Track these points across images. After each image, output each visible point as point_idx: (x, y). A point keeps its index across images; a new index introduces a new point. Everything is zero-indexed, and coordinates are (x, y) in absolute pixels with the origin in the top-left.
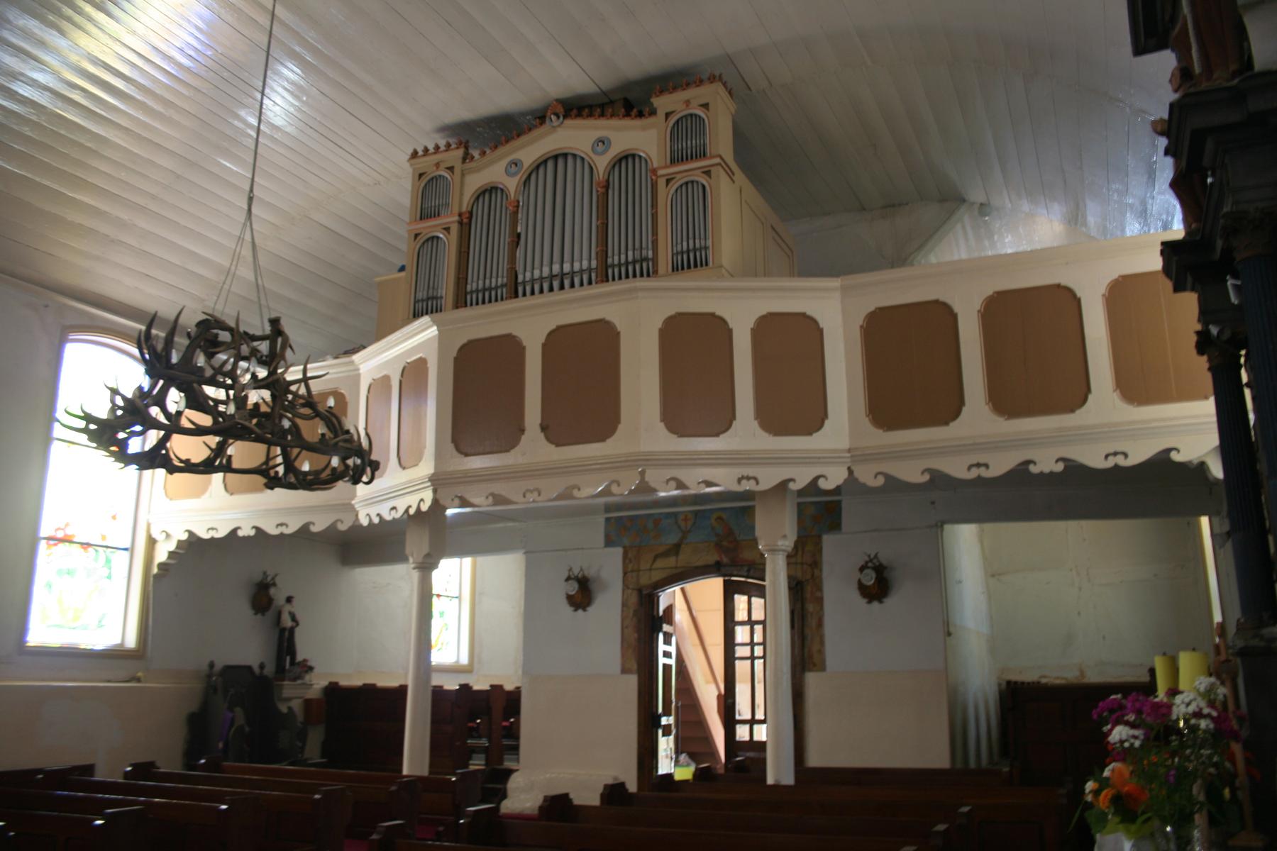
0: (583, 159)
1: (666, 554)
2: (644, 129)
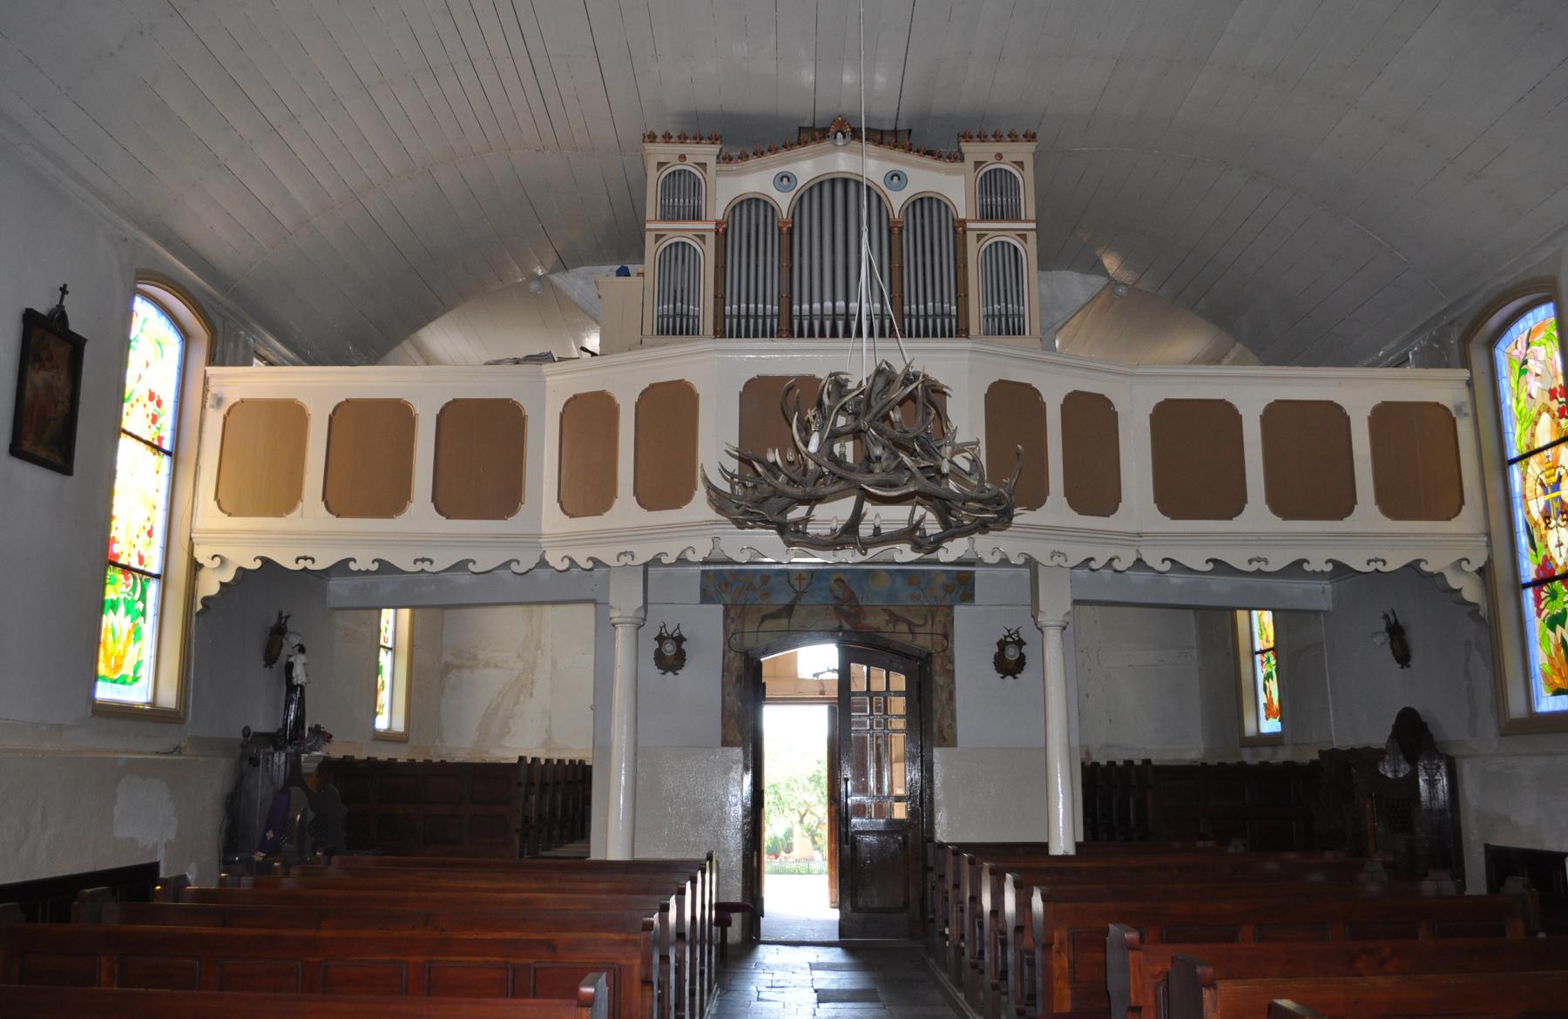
1: (775, 616)
2: (948, 173)
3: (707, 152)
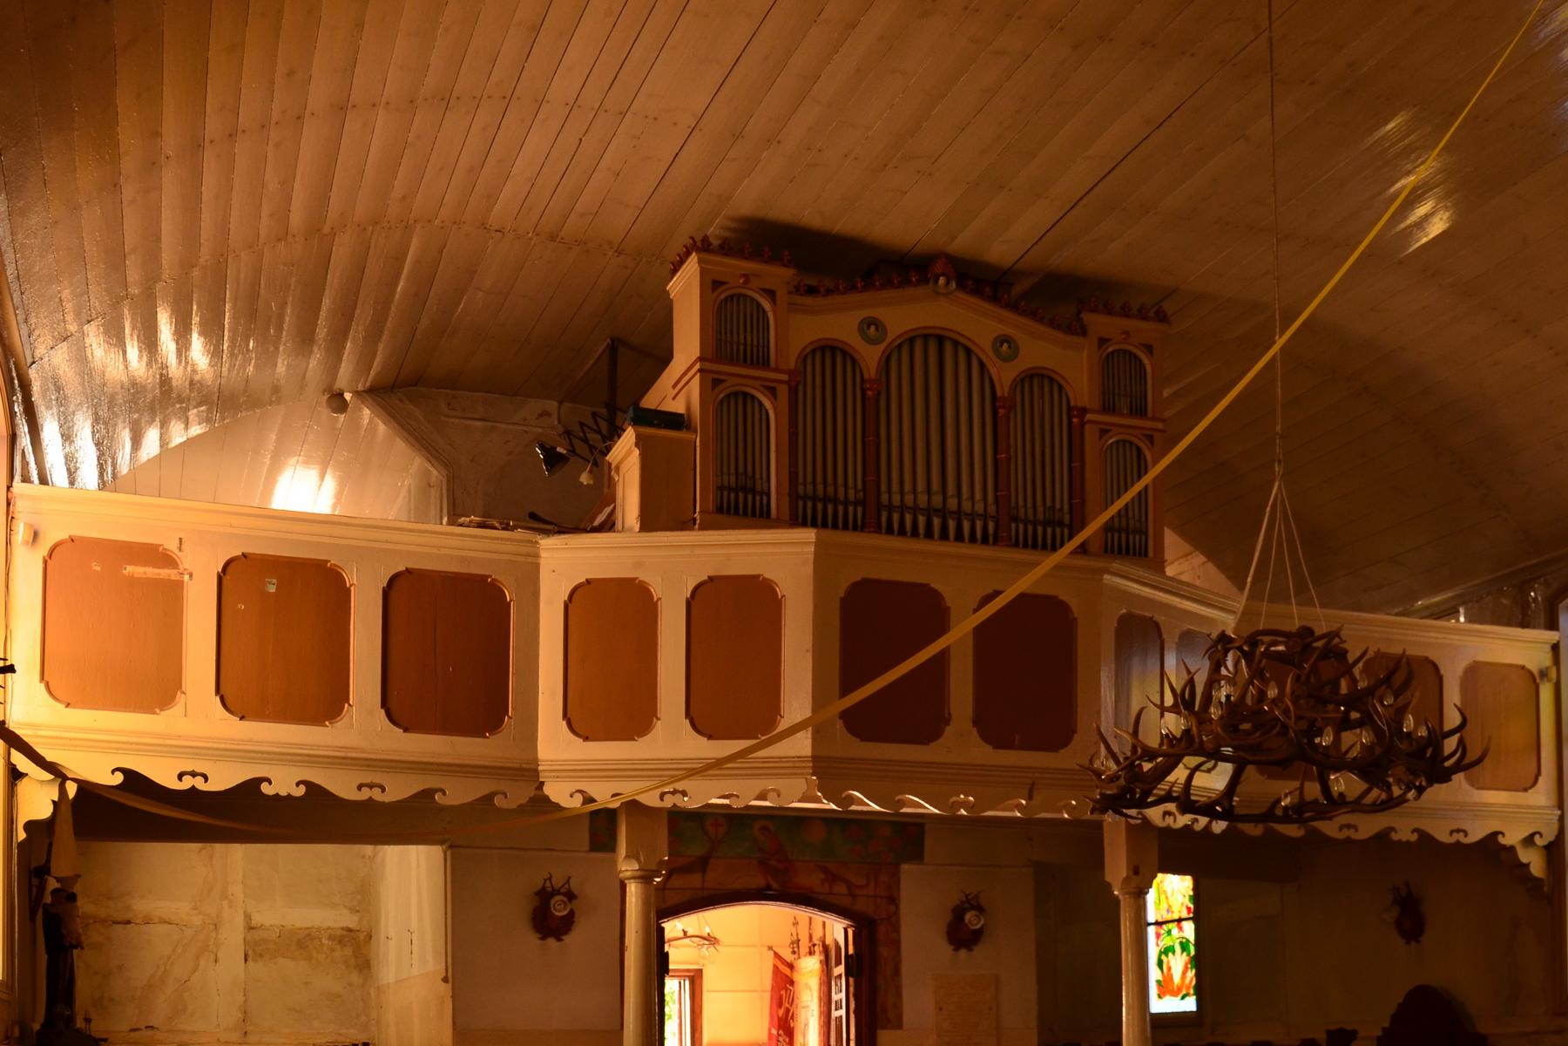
0: (968, 351)
3: (779, 275)
